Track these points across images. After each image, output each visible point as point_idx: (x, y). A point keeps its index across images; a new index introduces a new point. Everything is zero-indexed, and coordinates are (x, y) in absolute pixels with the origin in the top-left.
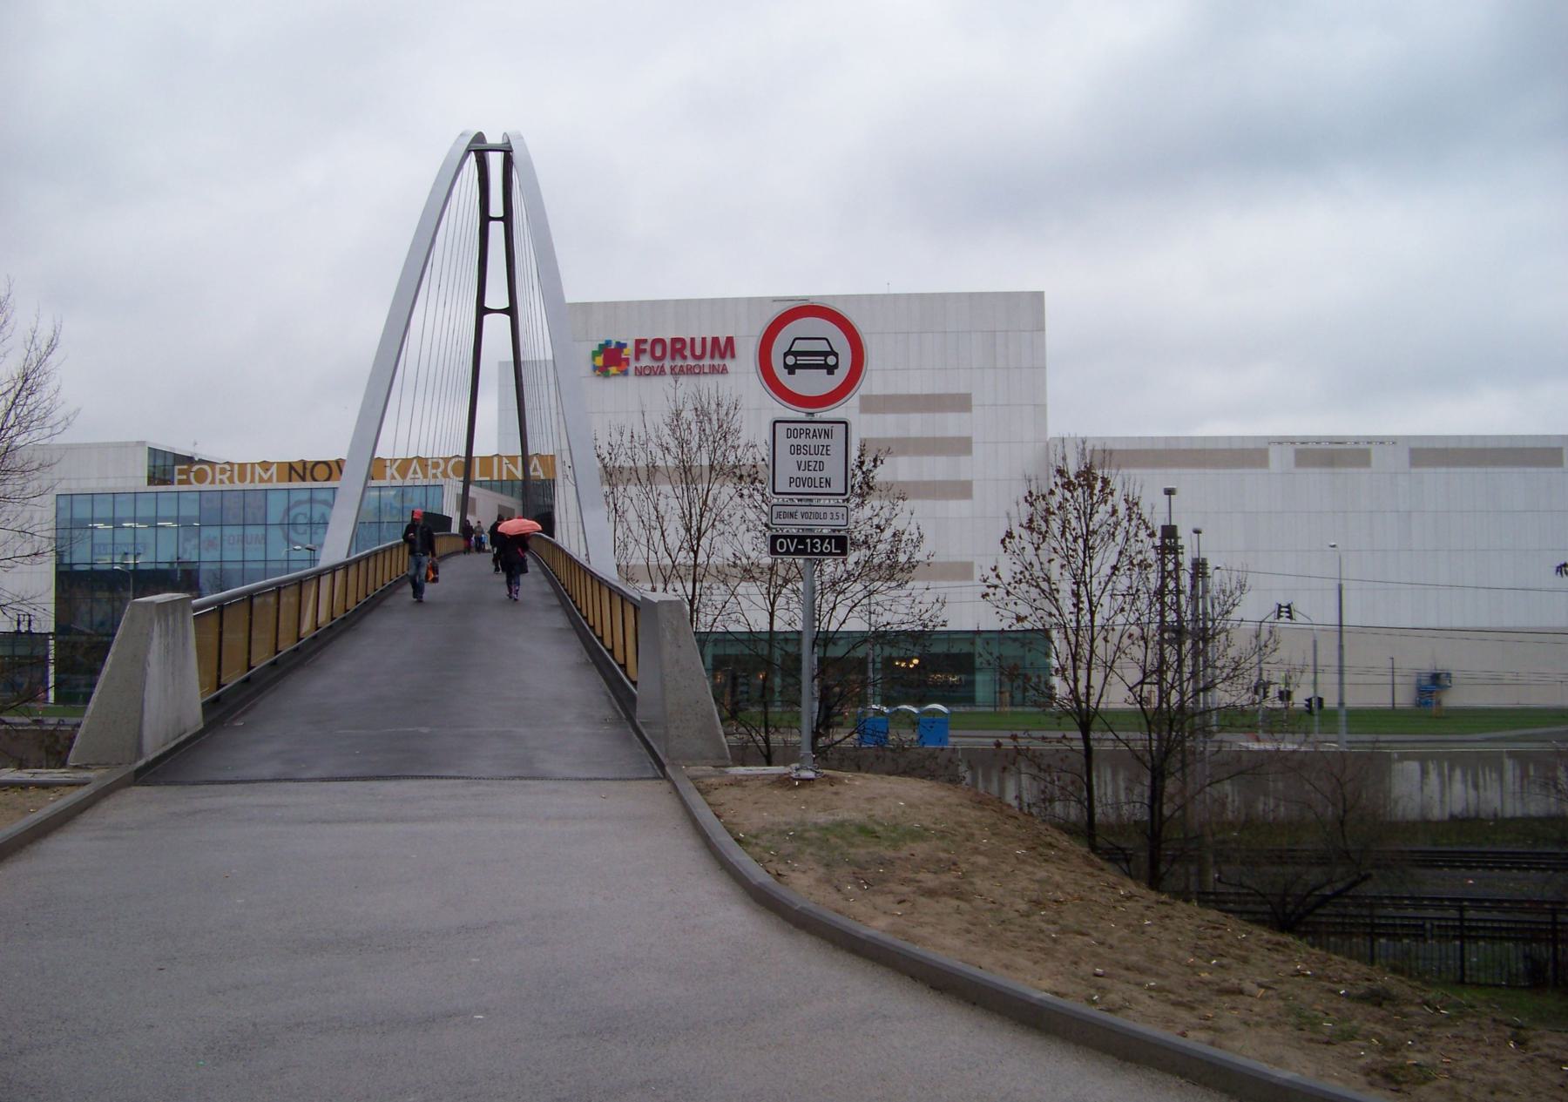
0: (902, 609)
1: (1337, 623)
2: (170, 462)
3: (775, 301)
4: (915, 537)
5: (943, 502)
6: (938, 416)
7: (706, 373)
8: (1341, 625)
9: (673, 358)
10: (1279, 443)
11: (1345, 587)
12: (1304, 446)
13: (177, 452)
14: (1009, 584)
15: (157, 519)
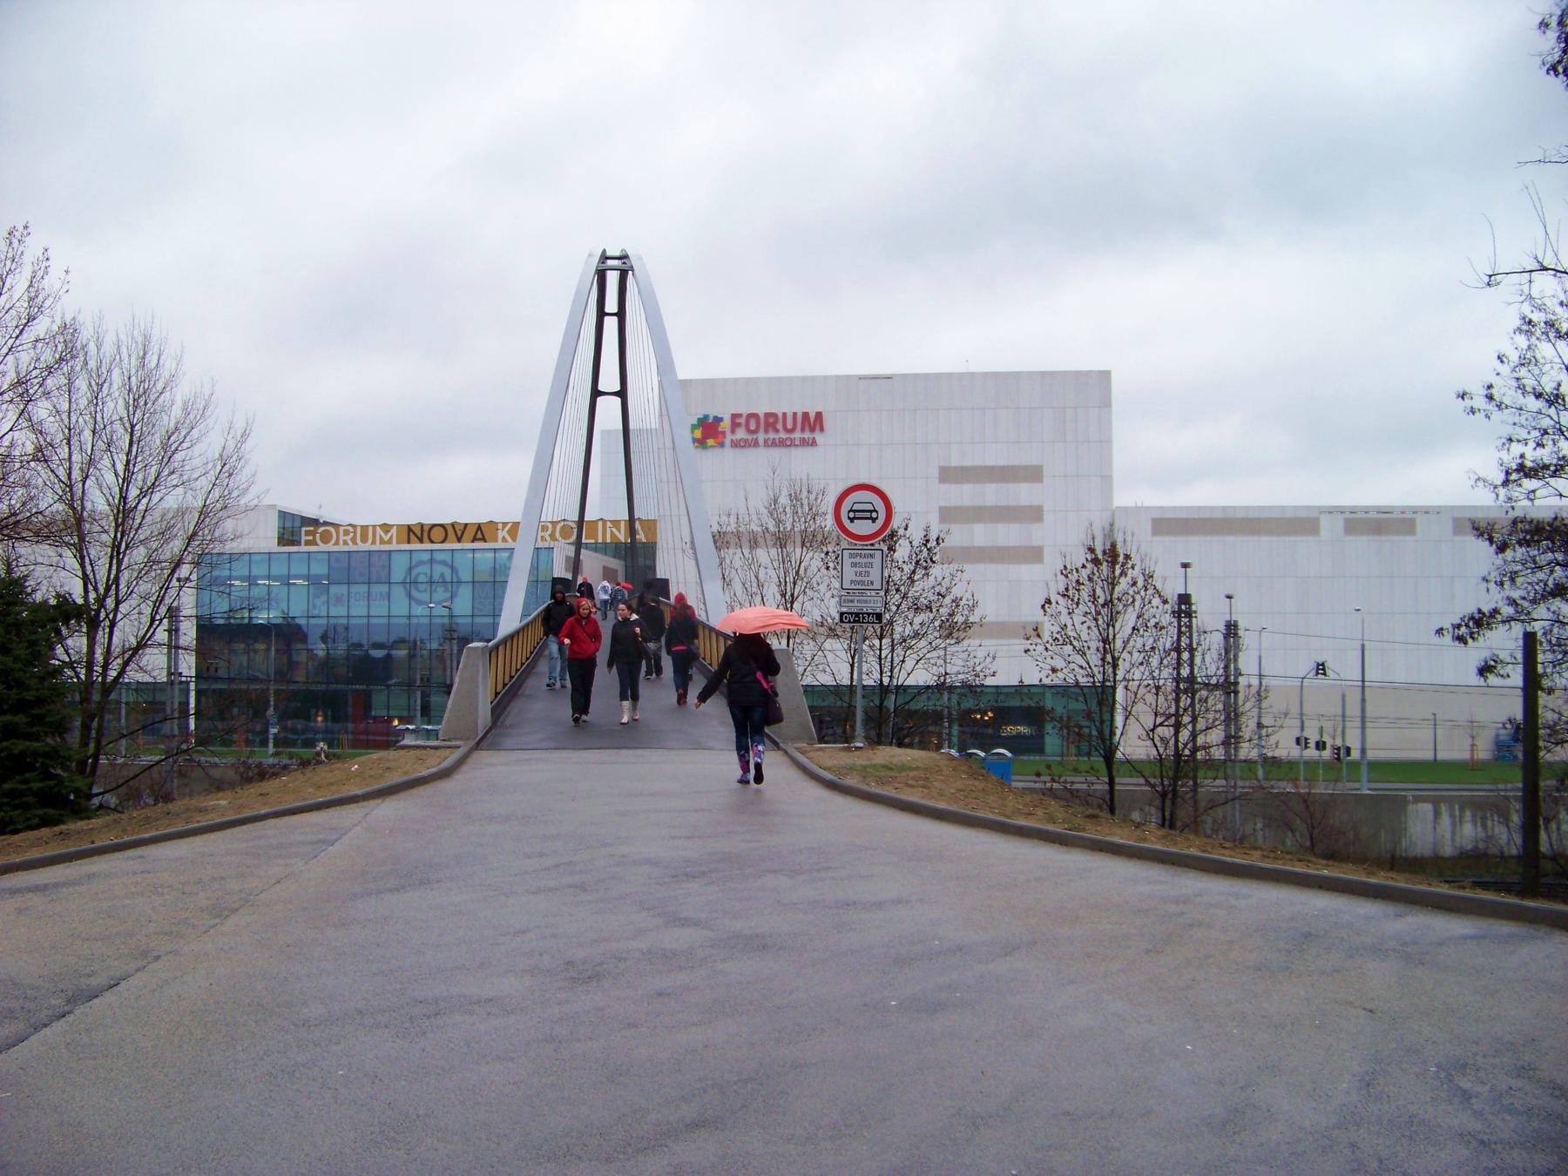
0: (960, 662)
1: (1360, 679)
2: (298, 524)
3: (860, 378)
4: (971, 603)
5: (1016, 566)
6: (1012, 486)
7: (797, 445)
8: (1363, 681)
9: (766, 431)
10: (1329, 512)
11: (1366, 648)
12: (1353, 516)
13: (303, 515)
14: (1048, 642)
15: (289, 577)
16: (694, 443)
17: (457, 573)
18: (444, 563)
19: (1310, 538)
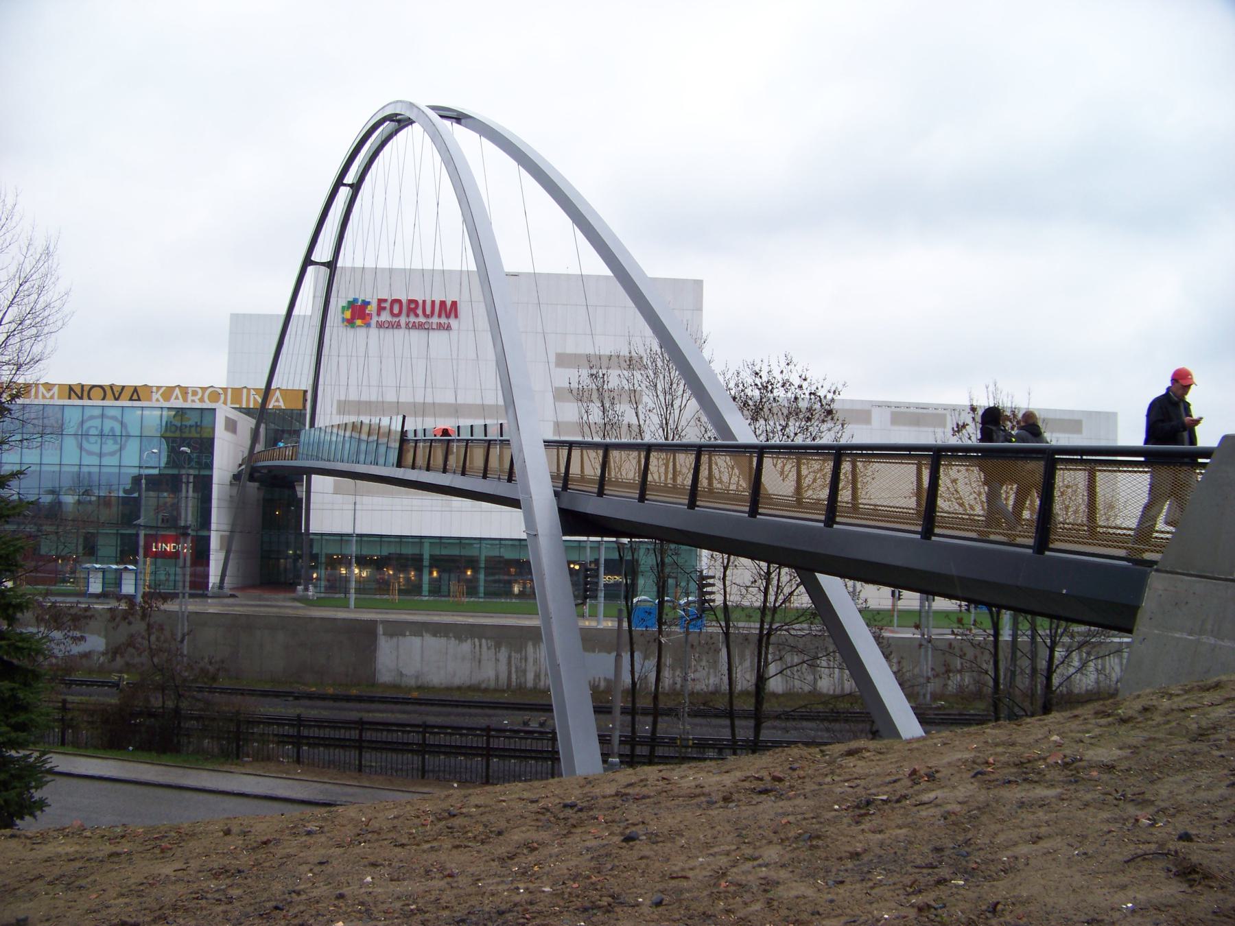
16: (343, 322)
17: (126, 428)
18: (114, 418)
19: (864, 427)
